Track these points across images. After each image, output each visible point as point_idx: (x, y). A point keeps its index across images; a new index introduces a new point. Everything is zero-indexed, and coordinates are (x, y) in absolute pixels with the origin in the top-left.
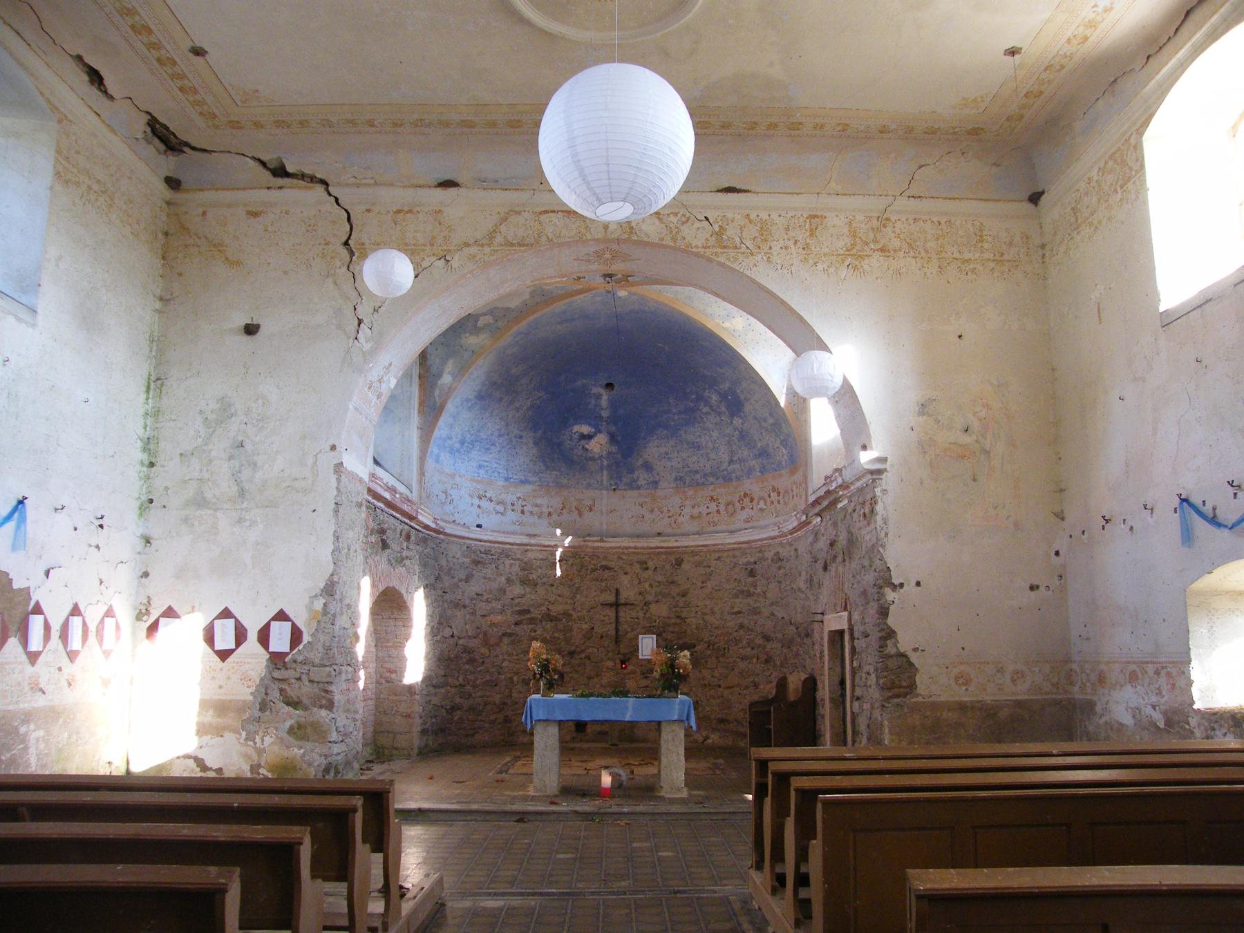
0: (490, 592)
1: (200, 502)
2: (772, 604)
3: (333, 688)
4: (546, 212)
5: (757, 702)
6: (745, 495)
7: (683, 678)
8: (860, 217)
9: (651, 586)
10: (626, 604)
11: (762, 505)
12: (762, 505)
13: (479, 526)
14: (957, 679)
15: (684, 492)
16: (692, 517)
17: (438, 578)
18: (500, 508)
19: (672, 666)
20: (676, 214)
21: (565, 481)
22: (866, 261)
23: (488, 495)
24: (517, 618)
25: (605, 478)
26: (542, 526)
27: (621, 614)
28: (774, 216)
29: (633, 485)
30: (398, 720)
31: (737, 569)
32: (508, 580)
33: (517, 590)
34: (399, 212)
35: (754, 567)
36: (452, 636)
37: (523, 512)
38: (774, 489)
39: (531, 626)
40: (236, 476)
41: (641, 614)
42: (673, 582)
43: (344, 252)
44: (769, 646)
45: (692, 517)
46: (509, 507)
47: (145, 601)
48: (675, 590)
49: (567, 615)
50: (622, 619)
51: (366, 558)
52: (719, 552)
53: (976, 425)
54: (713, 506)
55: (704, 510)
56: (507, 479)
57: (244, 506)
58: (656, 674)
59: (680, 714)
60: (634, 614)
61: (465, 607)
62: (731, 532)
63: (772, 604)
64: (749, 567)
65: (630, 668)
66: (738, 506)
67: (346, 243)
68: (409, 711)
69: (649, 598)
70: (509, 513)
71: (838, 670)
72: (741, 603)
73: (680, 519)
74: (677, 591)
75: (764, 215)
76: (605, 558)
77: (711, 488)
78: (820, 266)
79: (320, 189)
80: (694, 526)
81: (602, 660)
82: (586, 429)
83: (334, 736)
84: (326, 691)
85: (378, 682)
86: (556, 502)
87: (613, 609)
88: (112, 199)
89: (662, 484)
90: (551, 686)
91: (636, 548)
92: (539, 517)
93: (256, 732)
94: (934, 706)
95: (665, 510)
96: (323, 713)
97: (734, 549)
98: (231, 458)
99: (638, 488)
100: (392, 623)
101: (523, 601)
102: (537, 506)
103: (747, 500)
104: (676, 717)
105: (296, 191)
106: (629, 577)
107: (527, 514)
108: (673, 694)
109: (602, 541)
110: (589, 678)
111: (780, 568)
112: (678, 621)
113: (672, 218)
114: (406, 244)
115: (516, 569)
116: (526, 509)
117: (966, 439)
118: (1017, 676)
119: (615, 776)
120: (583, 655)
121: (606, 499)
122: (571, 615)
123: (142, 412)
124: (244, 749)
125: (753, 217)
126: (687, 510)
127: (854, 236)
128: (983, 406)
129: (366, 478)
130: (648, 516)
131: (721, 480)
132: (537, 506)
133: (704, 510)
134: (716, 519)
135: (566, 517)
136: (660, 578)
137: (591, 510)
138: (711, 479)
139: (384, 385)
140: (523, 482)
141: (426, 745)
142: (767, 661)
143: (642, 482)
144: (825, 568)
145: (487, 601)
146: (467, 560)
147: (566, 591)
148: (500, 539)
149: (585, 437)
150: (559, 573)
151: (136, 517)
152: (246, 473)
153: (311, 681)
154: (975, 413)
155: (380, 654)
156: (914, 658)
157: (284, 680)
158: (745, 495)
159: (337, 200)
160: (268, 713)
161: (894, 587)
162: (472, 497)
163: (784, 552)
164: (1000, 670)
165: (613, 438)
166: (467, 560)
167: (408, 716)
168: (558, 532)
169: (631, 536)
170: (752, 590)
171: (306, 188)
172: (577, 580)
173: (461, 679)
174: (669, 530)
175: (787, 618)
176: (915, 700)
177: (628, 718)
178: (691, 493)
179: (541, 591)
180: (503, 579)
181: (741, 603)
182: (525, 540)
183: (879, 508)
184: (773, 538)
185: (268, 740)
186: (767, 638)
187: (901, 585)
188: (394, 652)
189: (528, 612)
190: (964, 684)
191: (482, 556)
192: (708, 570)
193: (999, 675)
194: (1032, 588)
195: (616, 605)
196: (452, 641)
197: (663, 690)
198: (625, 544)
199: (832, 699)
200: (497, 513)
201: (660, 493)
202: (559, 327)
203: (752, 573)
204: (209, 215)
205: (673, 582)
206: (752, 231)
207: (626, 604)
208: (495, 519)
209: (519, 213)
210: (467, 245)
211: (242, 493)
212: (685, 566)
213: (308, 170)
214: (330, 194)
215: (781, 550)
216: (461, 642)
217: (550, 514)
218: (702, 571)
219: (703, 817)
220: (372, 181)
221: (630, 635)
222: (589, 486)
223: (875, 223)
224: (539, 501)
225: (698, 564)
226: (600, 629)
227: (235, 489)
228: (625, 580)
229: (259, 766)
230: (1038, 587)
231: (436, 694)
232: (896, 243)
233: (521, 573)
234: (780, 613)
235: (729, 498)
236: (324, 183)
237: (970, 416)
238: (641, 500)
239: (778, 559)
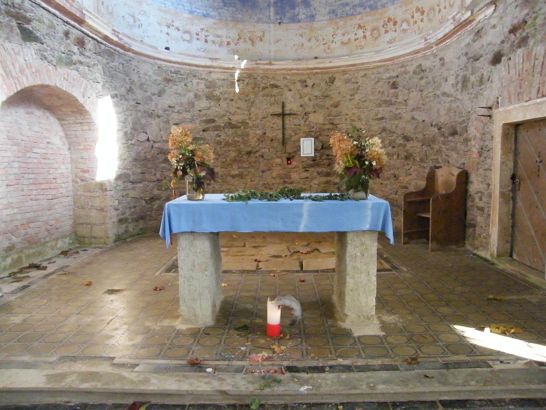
0: (181, 104)
2: (413, 110)
5: (412, 193)
6: (389, 20)
7: (376, 172)
9: (310, 100)
10: (290, 114)
11: (405, 26)
12: (405, 26)
13: (167, 48)
15: (336, 23)
16: (343, 43)
17: (130, 90)
18: (187, 37)
19: (360, 158)
21: (240, 16)
23: (176, 25)
24: (205, 126)
25: (272, 14)
26: (222, 52)
27: (287, 121)
29: (294, 19)
30: (93, 213)
31: (381, 83)
32: (196, 96)
33: (203, 103)
35: (395, 81)
36: (148, 140)
37: (206, 41)
38: (418, 10)
39: (216, 133)
41: (302, 122)
42: (327, 96)
44: (409, 145)
46: (195, 36)
48: (329, 103)
49: (244, 123)
50: (287, 126)
52: (364, 70)
54: (360, 33)
55: (353, 37)
56: (191, 12)
58: (339, 167)
59: (374, 221)
60: (297, 122)
61: (159, 117)
62: (377, 52)
63: (413, 110)
64: (392, 81)
65: (294, 163)
66: (382, 30)
68: (103, 205)
69: (309, 109)
70: (195, 41)
71: (511, 164)
72: (384, 111)
73: (333, 46)
74: (332, 102)
76: (274, 78)
77: (359, 17)
80: (344, 50)
81: (273, 158)
85: (74, 181)
86: (233, 34)
87: (281, 117)
89: (318, 17)
90: (199, 185)
91: (297, 69)
92: (220, 45)
95: (321, 38)
97: (378, 67)
99: (299, 21)
100: (78, 127)
101: (209, 112)
102: (218, 36)
104: (367, 227)
106: (292, 93)
107: (210, 43)
108: (361, 194)
109: (270, 64)
110: (263, 172)
111: (422, 78)
112: (331, 127)
115: (202, 86)
116: (209, 39)
119: (286, 310)
120: (258, 154)
121: (273, 31)
122: (248, 123)
126: (339, 38)
130: (307, 44)
131: (368, 10)
132: (218, 36)
133: (353, 37)
134: (363, 43)
135: (242, 46)
136: (317, 93)
137: (261, 40)
138: (359, 9)
140: (206, 16)
141: (127, 231)
142: (407, 158)
143: (302, 16)
145: (178, 112)
146: (160, 78)
147: (243, 105)
150: (237, 90)
155: (74, 157)
158: (389, 20)
162: (160, 24)
163: (426, 64)
166: (160, 78)
167: (102, 210)
168: (236, 57)
169: (294, 60)
170: (394, 99)
172: (252, 96)
173: (158, 175)
174: (325, 55)
175: (428, 121)
177: (301, 230)
178: (341, 23)
179: (223, 104)
180: (191, 95)
181: (384, 111)
182: (209, 63)
184: (417, 52)
186: (407, 139)
188: (85, 154)
189: (213, 121)
191: (172, 76)
192: (356, 86)
195: (283, 115)
196: (147, 144)
197: (348, 189)
198: (290, 67)
199: (502, 194)
200: (184, 40)
201: (316, 25)
203: (394, 86)
205: (327, 96)
207: (290, 114)
208: (184, 46)
212: (337, 83)
215: (422, 62)
216: (156, 145)
217: (228, 43)
218: (351, 86)
221: (293, 139)
222: (259, 21)
224: (219, 32)
225: (347, 81)
226: (270, 134)
228: (289, 95)
231: (134, 189)
233: (207, 90)
234: (420, 116)
235: (375, 24)
238: (301, 32)
239: (421, 70)
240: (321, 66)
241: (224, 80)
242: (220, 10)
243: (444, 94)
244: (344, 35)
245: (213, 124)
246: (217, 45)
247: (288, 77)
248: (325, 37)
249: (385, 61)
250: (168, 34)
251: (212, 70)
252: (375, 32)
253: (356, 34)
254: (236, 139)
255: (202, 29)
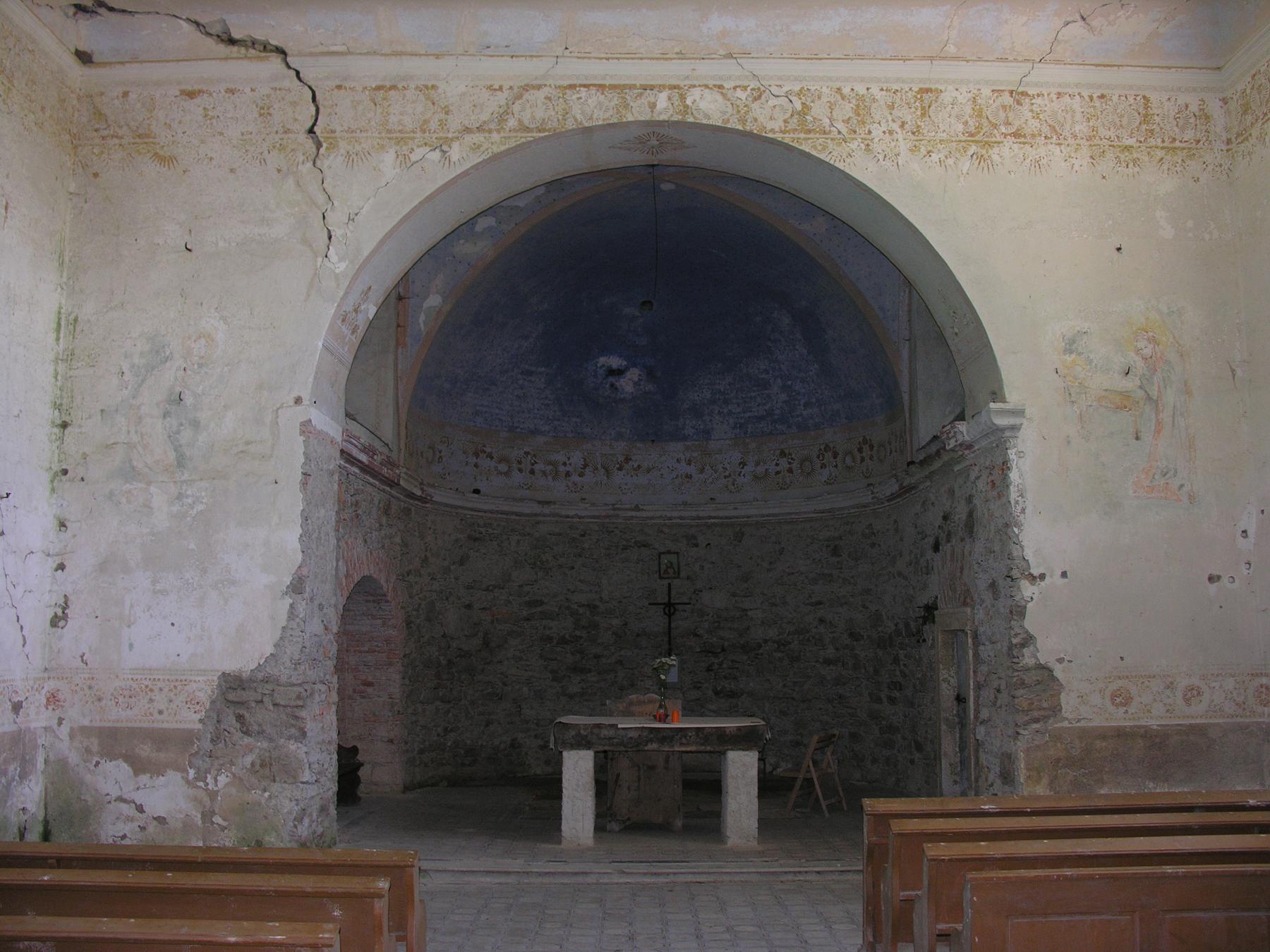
1: (129, 473)
3: (303, 714)
4: (572, 87)
8: (986, 92)
9: (702, 568)
13: (477, 491)
14: (1114, 696)
16: (756, 477)
18: (503, 467)
20: (745, 88)
22: (996, 150)
28: (875, 90)
34: (379, 88)
38: (865, 441)
40: (172, 437)
43: (309, 144)
45: (756, 477)
47: (61, 602)
51: (338, 540)
53: (1139, 364)
54: (784, 463)
57: (186, 476)
67: (311, 131)
70: (515, 473)
75: (861, 90)
78: (935, 157)
79: (276, 61)
82: (615, 362)
83: (307, 776)
84: (297, 718)
88: (10, 82)
91: (681, 518)
93: (207, 771)
94: (1084, 733)
96: (292, 746)
97: (811, 520)
98: (166, 415)
99: (685, 438)
102: (550, 463)
103: (829, 455)
105: (245, 63)
111: (873, 545)
113: (739, 93)
114: (389, 131)
116: (536, 467)
117: (1130, 384)
118: (1192, 693)
123: (52, 356)
124: (191, 792)
125: (846, 91)
127: (980, 116)
128: (1148, 339)
129: (339, 439)
133: (773, 469)
139: (360, 316)
144: (936, 548)
148: (506, 508)
149: (612, 372)
151: (48, 493)
152: (186, 435)
153: (275, 705)
154: (1138, 351)
156: (1058, 672)
157: (241, 703)
158: (827, 448)
159: (298, 73)
160: (221, 745)
161: (1032, 578)
164: (1170, 686)
165: (650, 373)
171: (259, 58)
176: (1059, 725)
182: (537, 509)
183: (1014, 475)
185: (223, 779)
187: (1042, 577)
189: (542, 603)
190: (1122, 704)
193: (1168, 692)
194: (1211, 579)
202: (947, 692)
203: (836, 551)
204: (132, 96)
206: (847, 109)
209: (539, 87)
210: (467, 130)
211: (181, 462)
213: (259, 36)
214: (289, 67)
219: (783, 878)
220: (343, 49)
223: (1007, 99)
227: (172, 456)
229: (213, 813)
230: (1219, 577)
232: (1033, 125)
236: (282, 52)
237: (1133, 354)
240: (721, 514)
241: (560, 534)
242: (556, 423)
243: (900, 574)
244: (757, 464)
245: (539, 609)
246: (550, 478)
247: (667, 530)
248: (727, 466)
249: (910, 410)
250: (476, 466)
251: (541, 518)
252: (807, 463)
253: (777, 465)
254: (578, 633)
255: (527, 453)
